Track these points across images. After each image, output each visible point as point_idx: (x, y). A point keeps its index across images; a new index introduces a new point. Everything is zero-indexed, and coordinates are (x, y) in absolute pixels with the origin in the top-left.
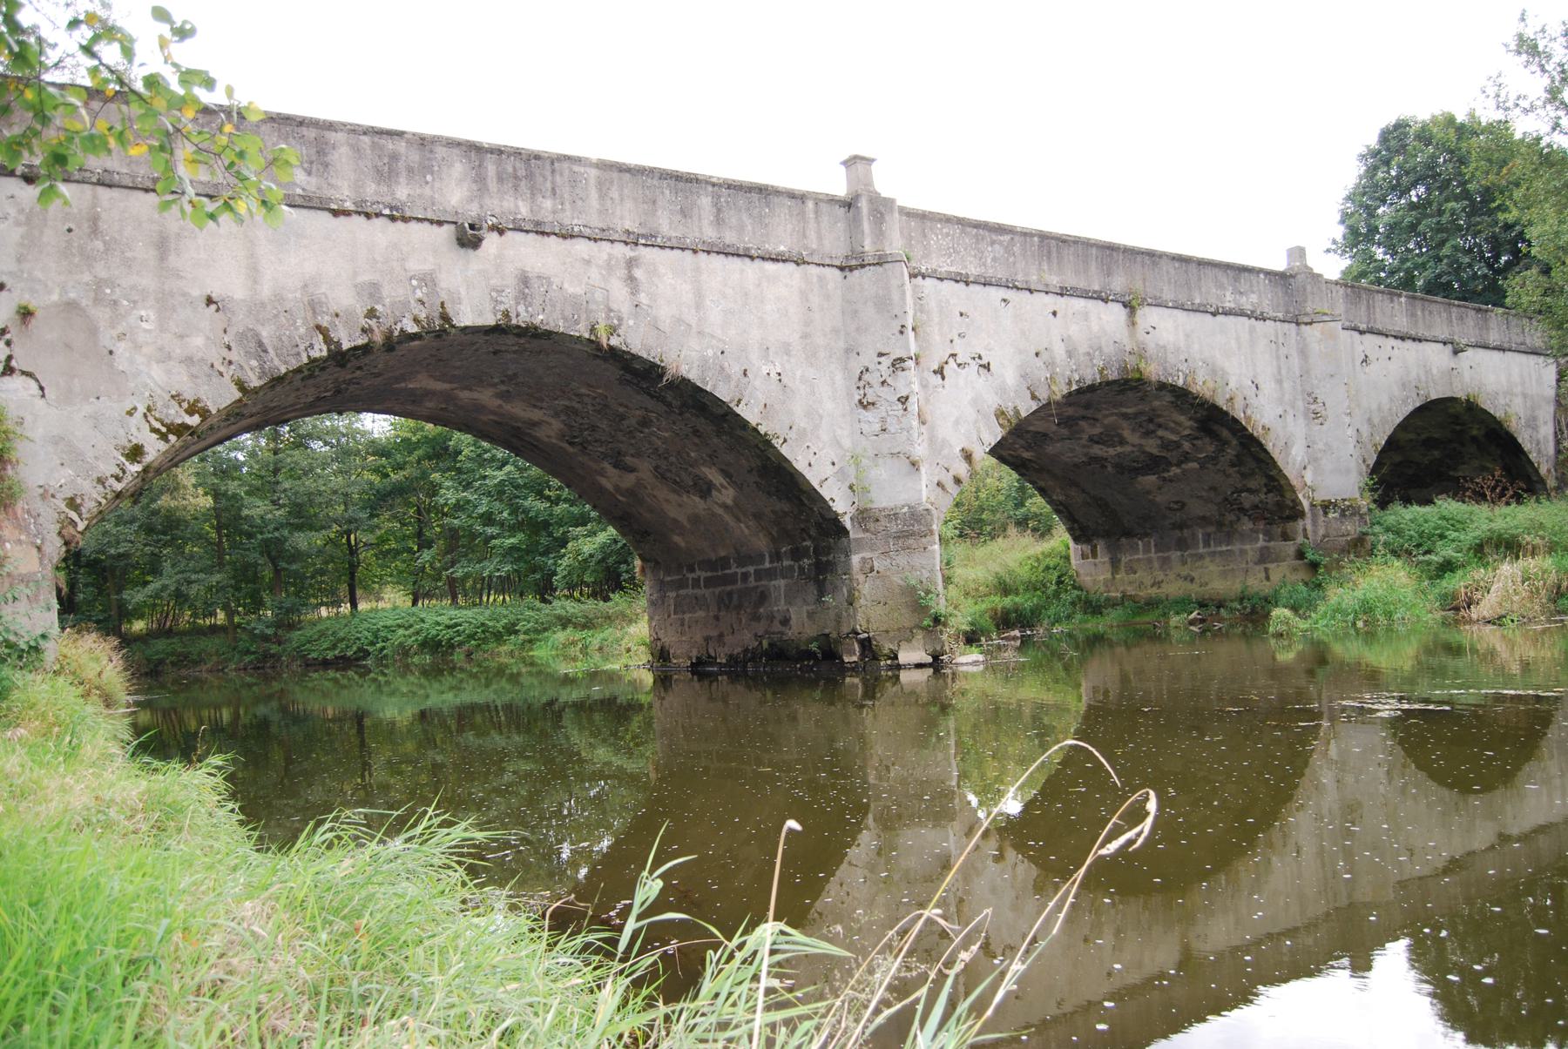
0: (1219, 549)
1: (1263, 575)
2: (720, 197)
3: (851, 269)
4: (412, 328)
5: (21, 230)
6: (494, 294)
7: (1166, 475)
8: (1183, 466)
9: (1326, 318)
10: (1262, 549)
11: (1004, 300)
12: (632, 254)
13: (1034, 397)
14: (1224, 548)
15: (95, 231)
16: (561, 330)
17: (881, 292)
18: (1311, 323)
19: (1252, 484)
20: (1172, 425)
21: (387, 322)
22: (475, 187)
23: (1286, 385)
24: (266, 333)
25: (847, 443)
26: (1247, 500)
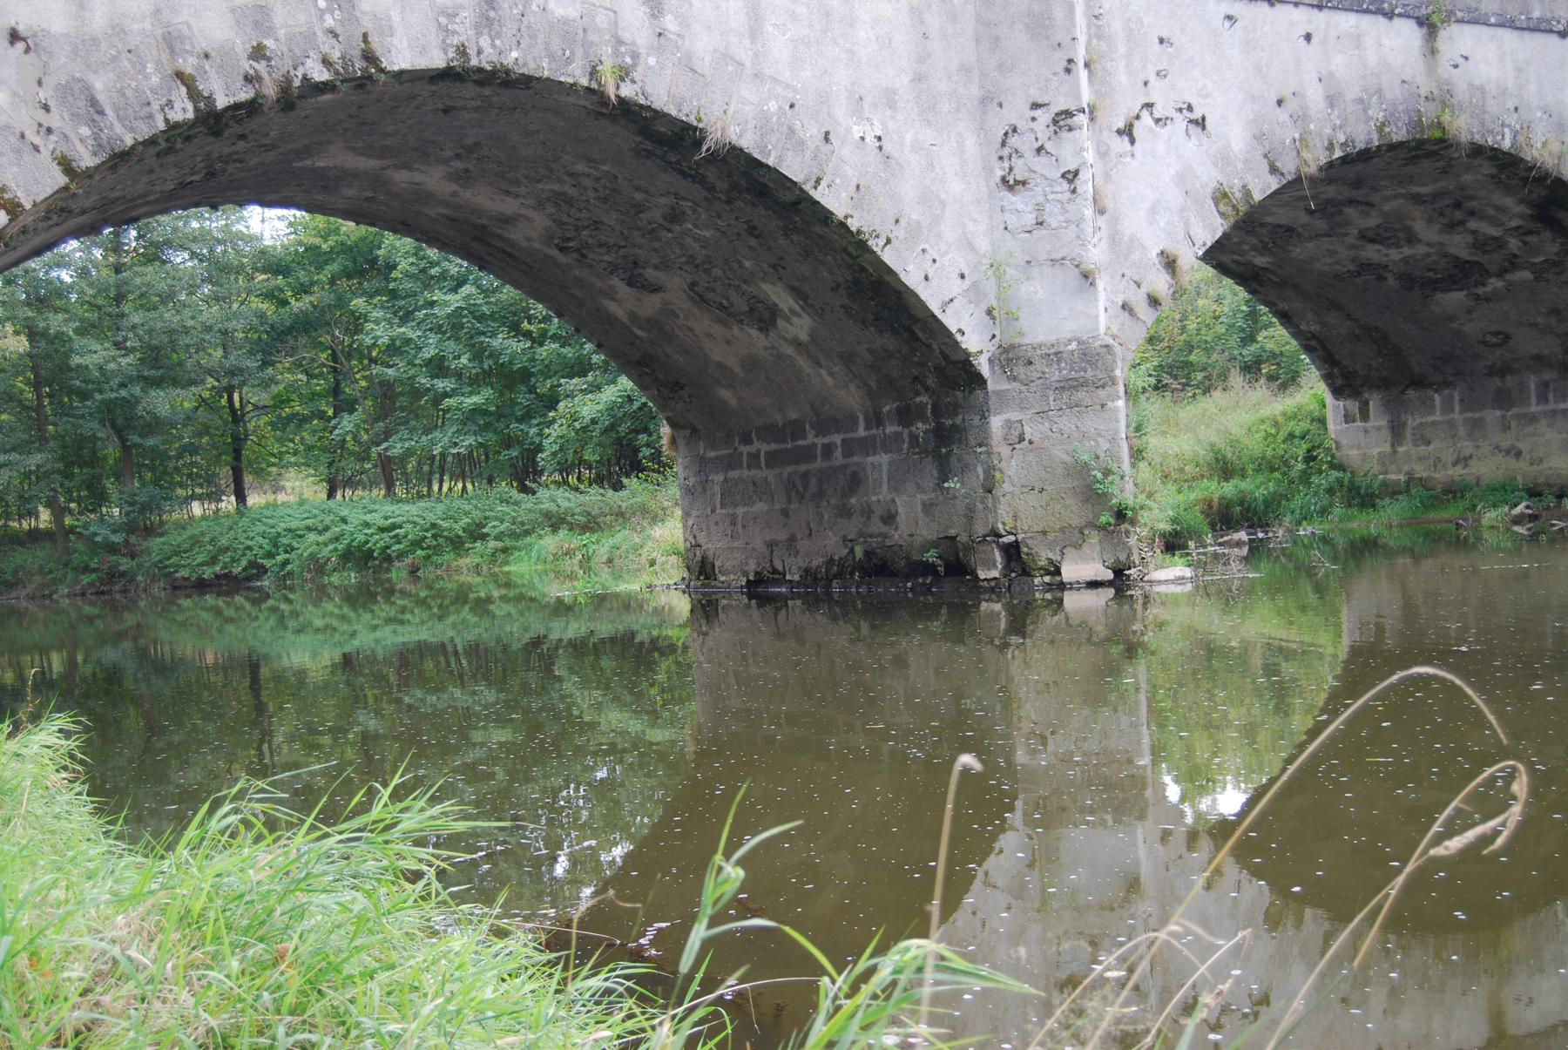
4: (320, 75)
6: (443, 20)
7: (1480, 290)
8: (1508, 276)
11: (1229, 18)
13: (1274, 170)
16: (546, 74)
20: (1491, 212)
21: (282, 65)
24: (101, 85)
25: (983, 244)
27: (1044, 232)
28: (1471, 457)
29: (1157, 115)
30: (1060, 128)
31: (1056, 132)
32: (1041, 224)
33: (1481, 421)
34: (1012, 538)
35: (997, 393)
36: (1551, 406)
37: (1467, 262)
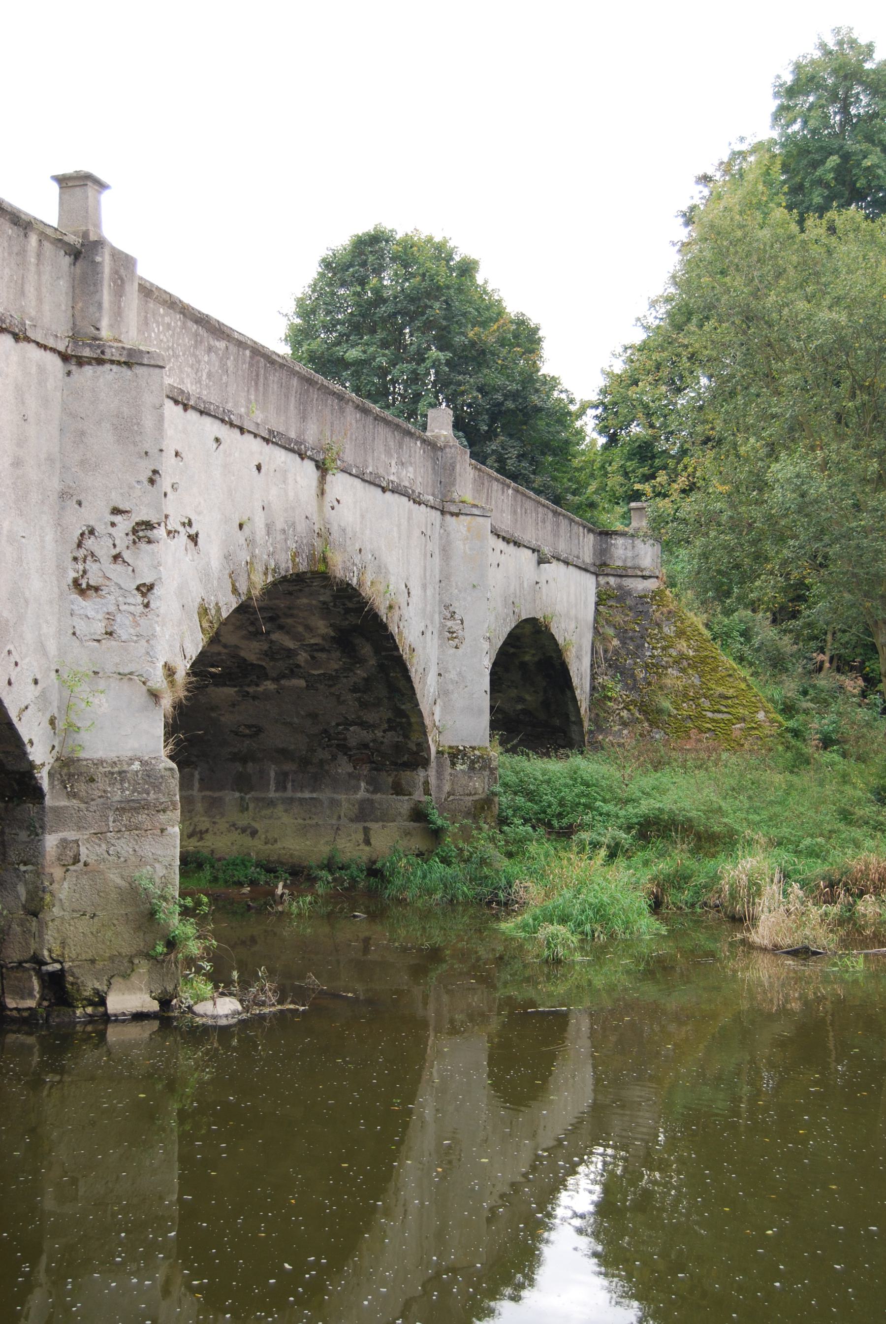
0: (299, 795)
1: (360, 837)
3: (81, 362)
7: (251, 690)
8: (282, 682)
9: (475, 511)
10: (362, 802)
11: (217, 440)
13: (235, 590)
14: (307, 795)
17: (125, 410)
18: (457, 515)
19: (370, 717)
20: (300, 629)
23: (429, 593)
25: (52, 647)
26: (355, 735)
27: (113, 643)
28: (207, 831)
29: (169, 528)
30: (139, 538)
31: (134, 542)
32: (111, 634)
33: (220, 799)
34: (58, 966)
35: (55, 809)
36: (289, 794)
37: (252, 665)
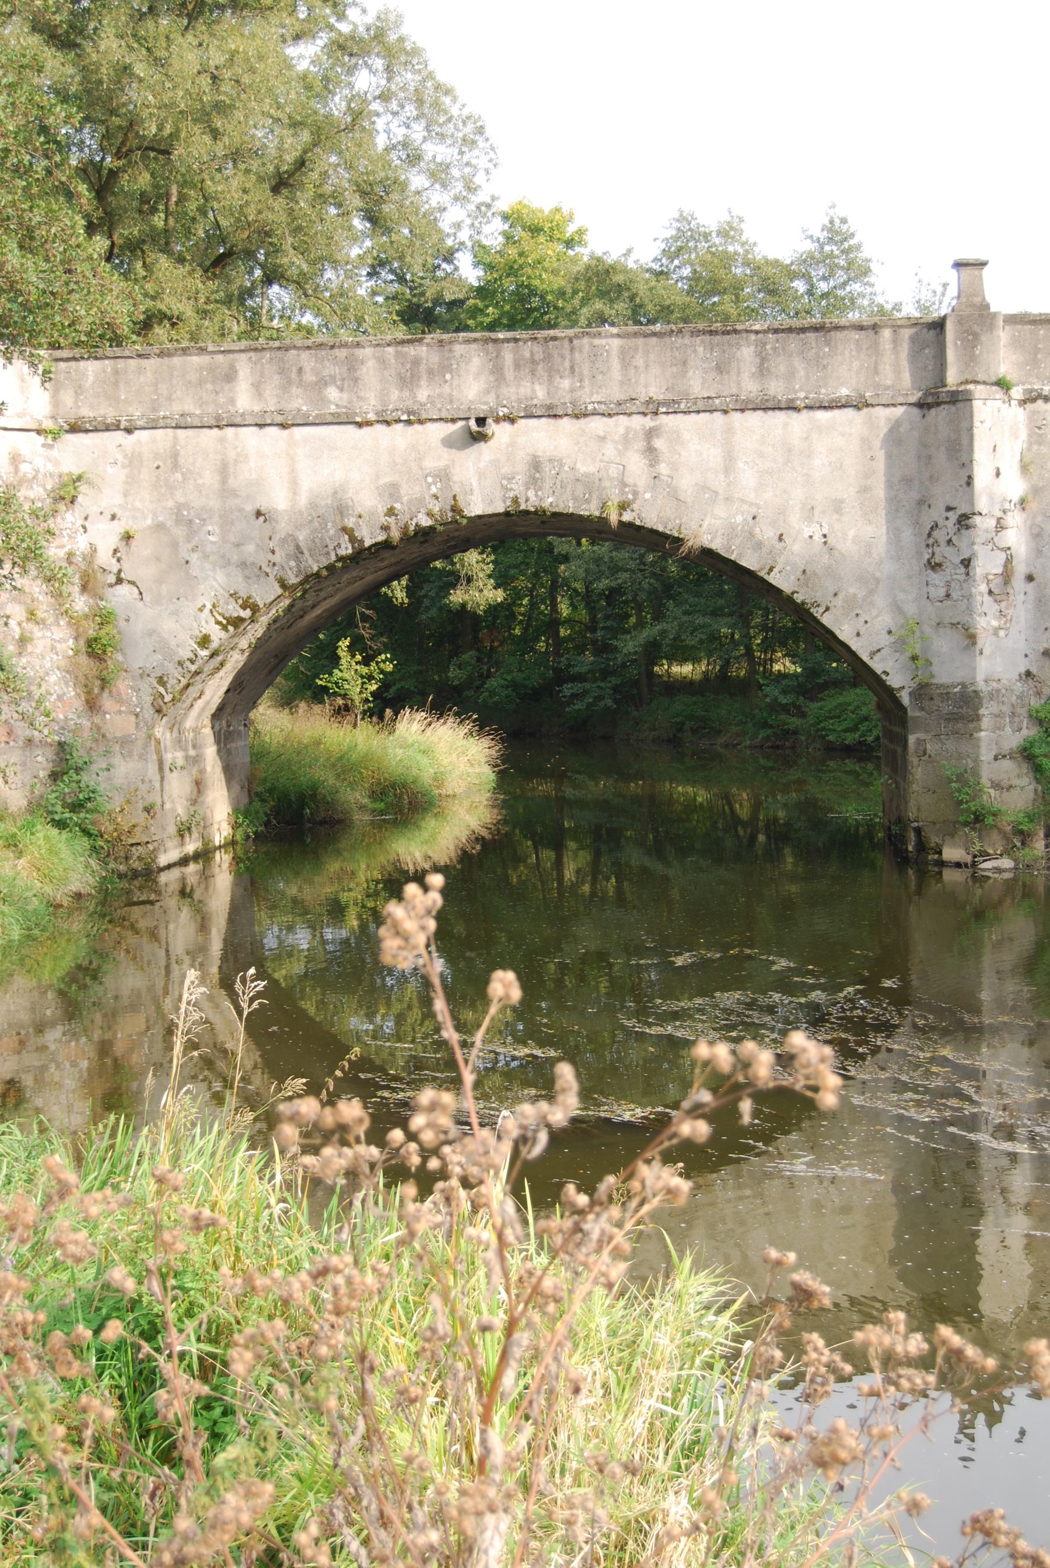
2: (765, 344)
4: (426, 522)
5: (126, 471)
6: (505, 482)
12: (652, 424)
15: (176, 466)
16: (571, 511)
21: (404, 518)
22: (492, 378)
24: (302, 536)
25: (911, 609)
